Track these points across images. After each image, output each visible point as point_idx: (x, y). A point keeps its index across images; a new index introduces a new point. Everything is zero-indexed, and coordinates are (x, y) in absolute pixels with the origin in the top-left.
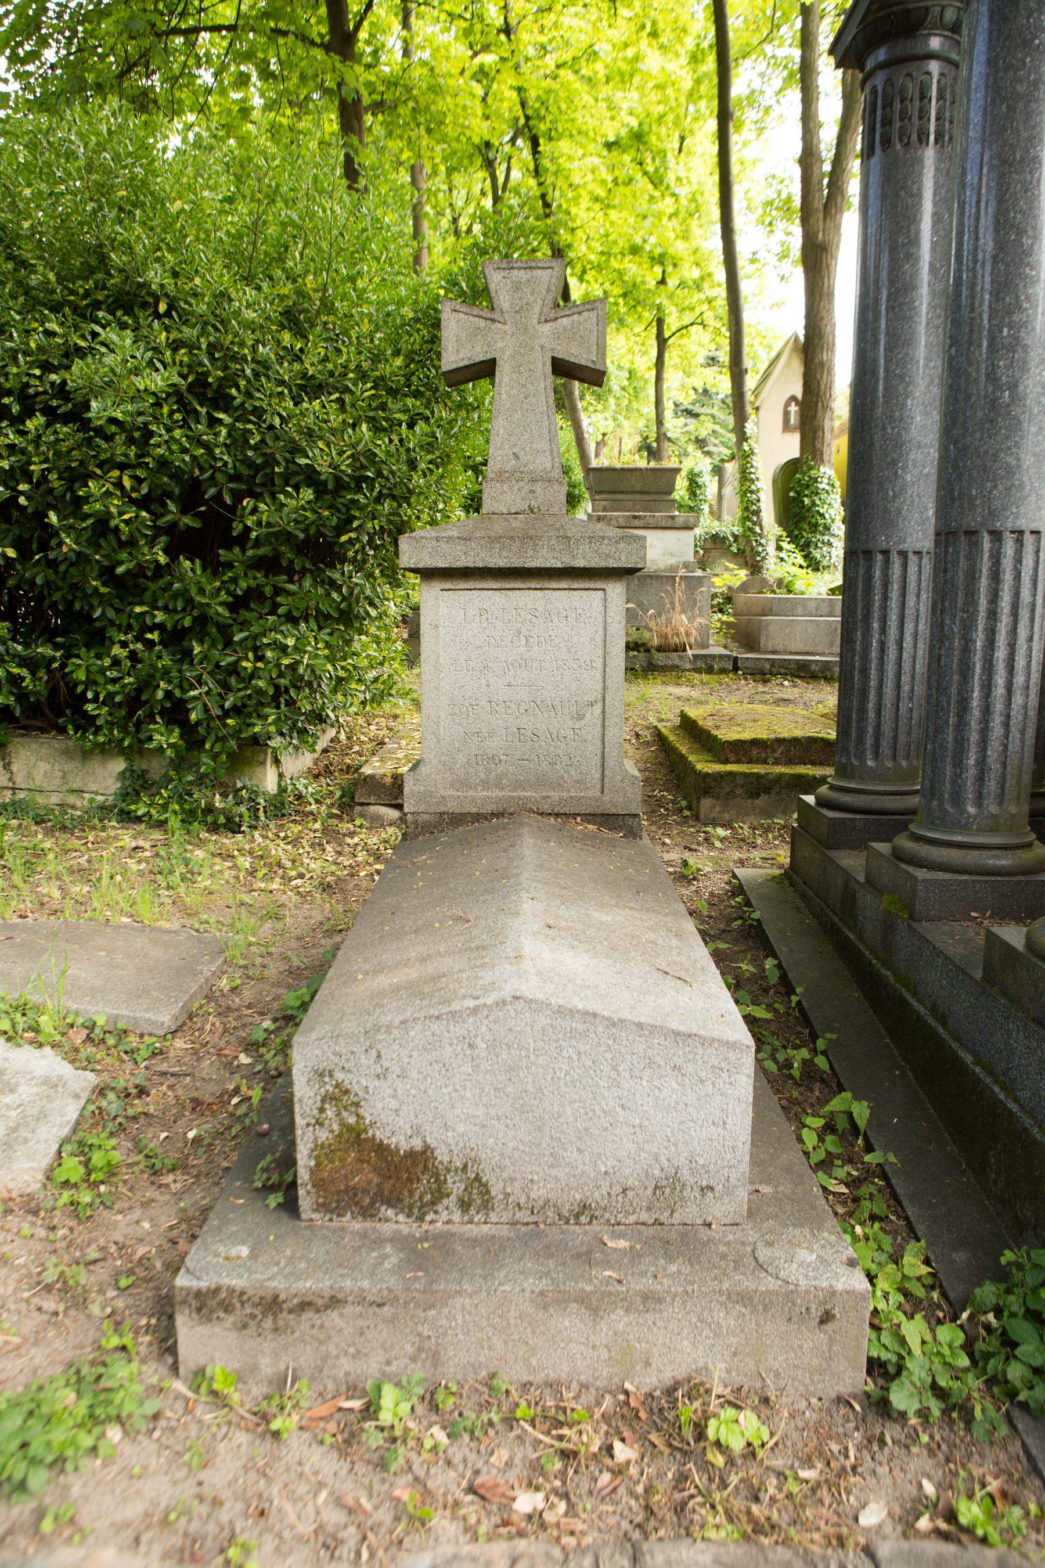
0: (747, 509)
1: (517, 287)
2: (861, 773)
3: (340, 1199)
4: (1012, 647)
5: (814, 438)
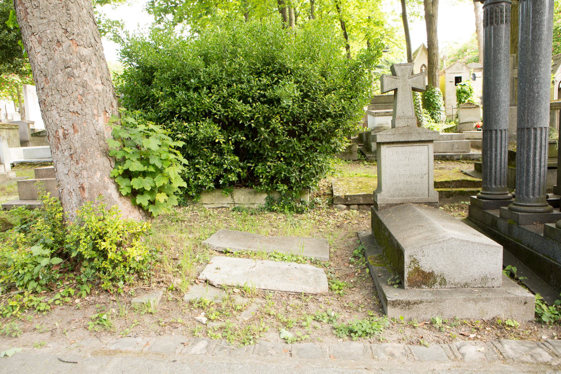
0: (415, 105)
1: (402, 70)
2: (491, 189)
3: (414, 284)
4: (540, 156)
5: (433, 78)
